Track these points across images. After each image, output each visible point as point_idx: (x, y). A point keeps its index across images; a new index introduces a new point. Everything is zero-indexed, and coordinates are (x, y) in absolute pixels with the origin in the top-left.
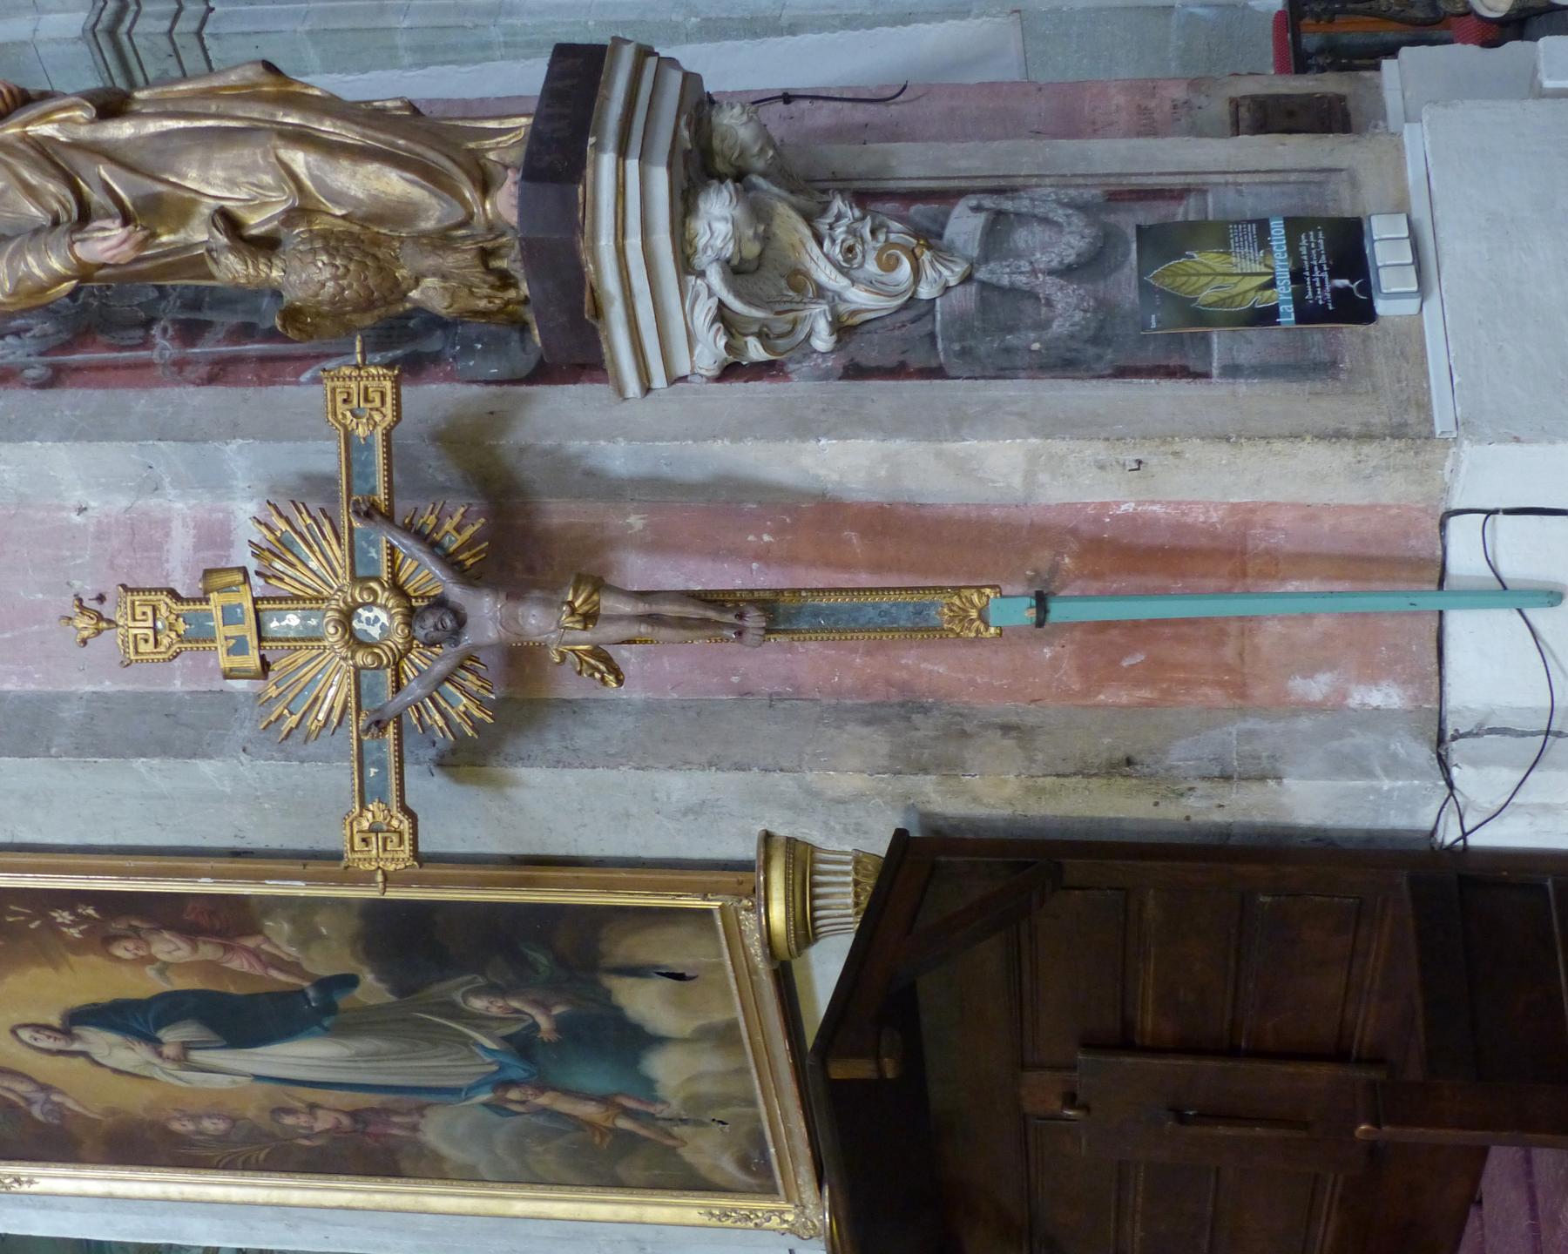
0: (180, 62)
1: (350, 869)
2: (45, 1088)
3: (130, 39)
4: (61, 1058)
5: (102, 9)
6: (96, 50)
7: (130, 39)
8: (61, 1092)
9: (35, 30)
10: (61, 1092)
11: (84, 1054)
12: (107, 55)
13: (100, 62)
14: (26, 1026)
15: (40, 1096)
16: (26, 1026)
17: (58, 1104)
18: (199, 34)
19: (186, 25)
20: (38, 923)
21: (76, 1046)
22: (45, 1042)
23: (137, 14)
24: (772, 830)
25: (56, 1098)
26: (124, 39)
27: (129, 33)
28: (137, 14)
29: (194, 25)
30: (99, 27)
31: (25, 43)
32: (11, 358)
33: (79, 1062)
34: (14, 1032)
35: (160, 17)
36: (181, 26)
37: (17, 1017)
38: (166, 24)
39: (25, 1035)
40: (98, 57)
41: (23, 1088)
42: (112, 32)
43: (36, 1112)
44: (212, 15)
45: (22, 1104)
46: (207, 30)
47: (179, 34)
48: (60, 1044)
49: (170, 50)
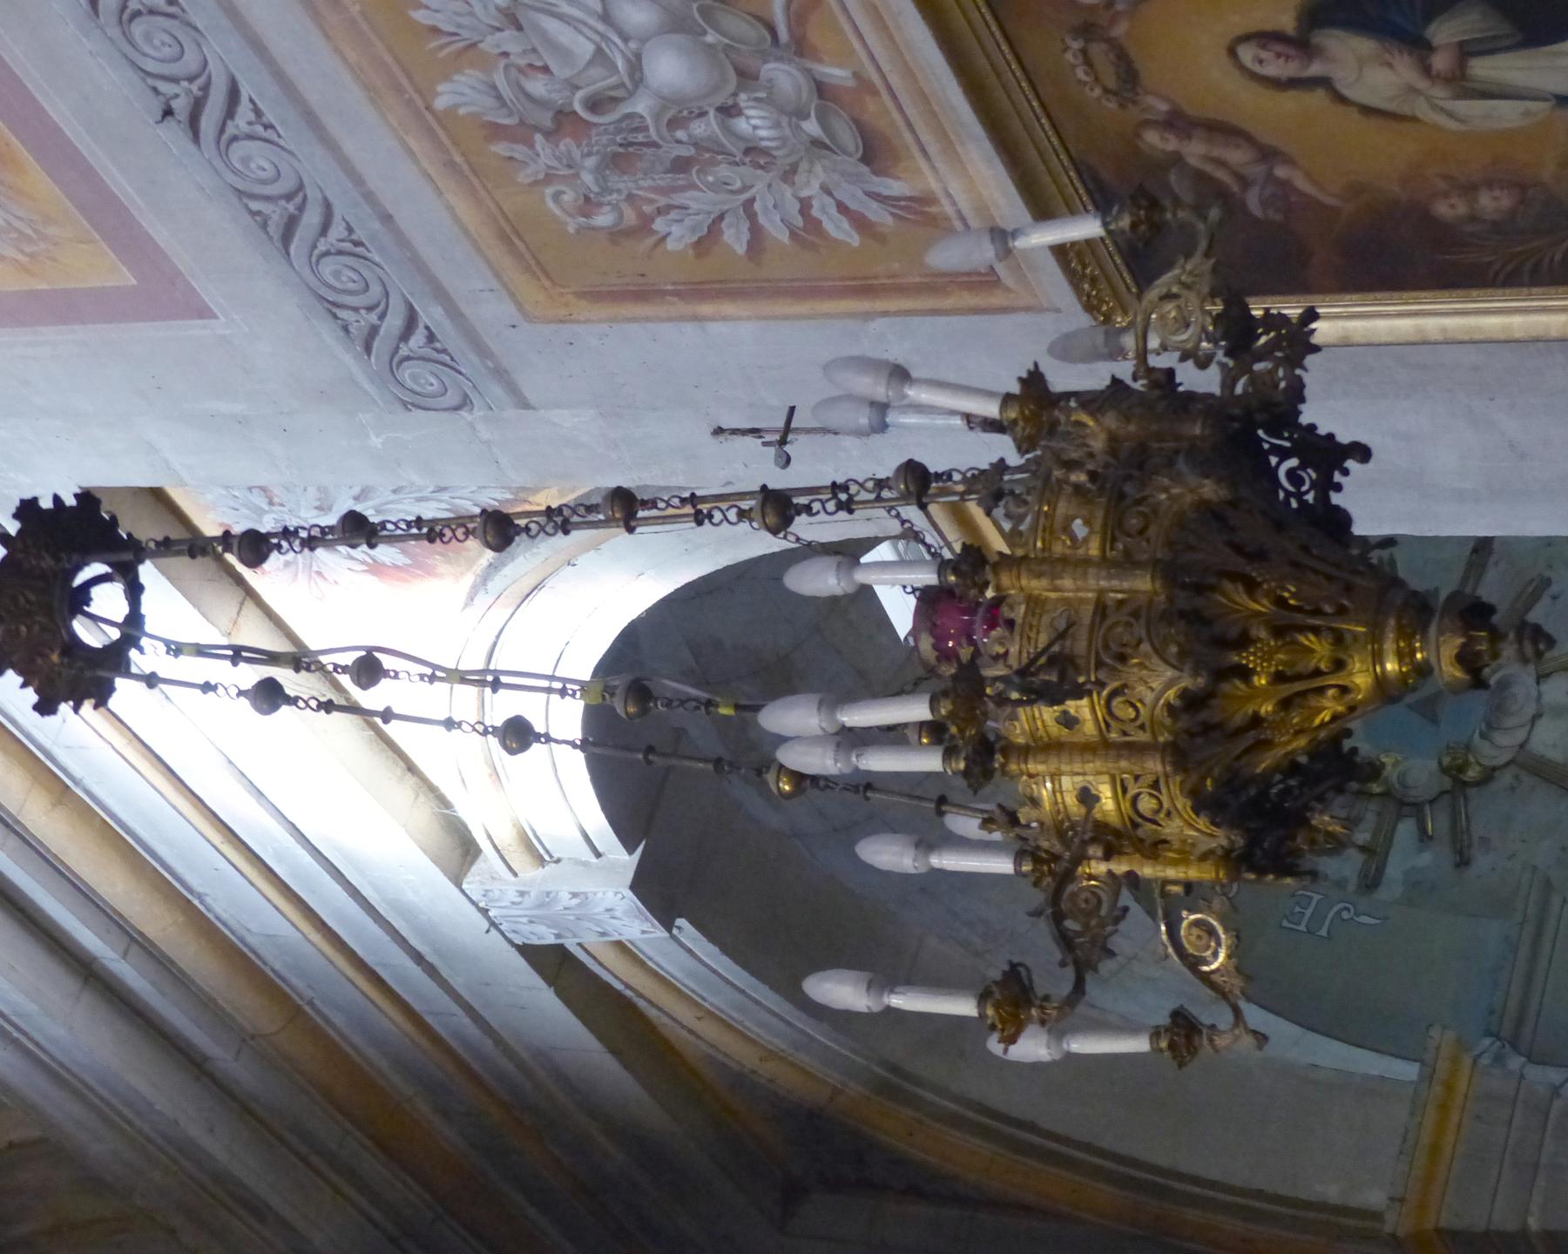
2: (1268, 154)
11: (1324, 82)
21: (1315, 69)
25: (1281, 172)
39: (1247, 54)
41: (1238, 156)
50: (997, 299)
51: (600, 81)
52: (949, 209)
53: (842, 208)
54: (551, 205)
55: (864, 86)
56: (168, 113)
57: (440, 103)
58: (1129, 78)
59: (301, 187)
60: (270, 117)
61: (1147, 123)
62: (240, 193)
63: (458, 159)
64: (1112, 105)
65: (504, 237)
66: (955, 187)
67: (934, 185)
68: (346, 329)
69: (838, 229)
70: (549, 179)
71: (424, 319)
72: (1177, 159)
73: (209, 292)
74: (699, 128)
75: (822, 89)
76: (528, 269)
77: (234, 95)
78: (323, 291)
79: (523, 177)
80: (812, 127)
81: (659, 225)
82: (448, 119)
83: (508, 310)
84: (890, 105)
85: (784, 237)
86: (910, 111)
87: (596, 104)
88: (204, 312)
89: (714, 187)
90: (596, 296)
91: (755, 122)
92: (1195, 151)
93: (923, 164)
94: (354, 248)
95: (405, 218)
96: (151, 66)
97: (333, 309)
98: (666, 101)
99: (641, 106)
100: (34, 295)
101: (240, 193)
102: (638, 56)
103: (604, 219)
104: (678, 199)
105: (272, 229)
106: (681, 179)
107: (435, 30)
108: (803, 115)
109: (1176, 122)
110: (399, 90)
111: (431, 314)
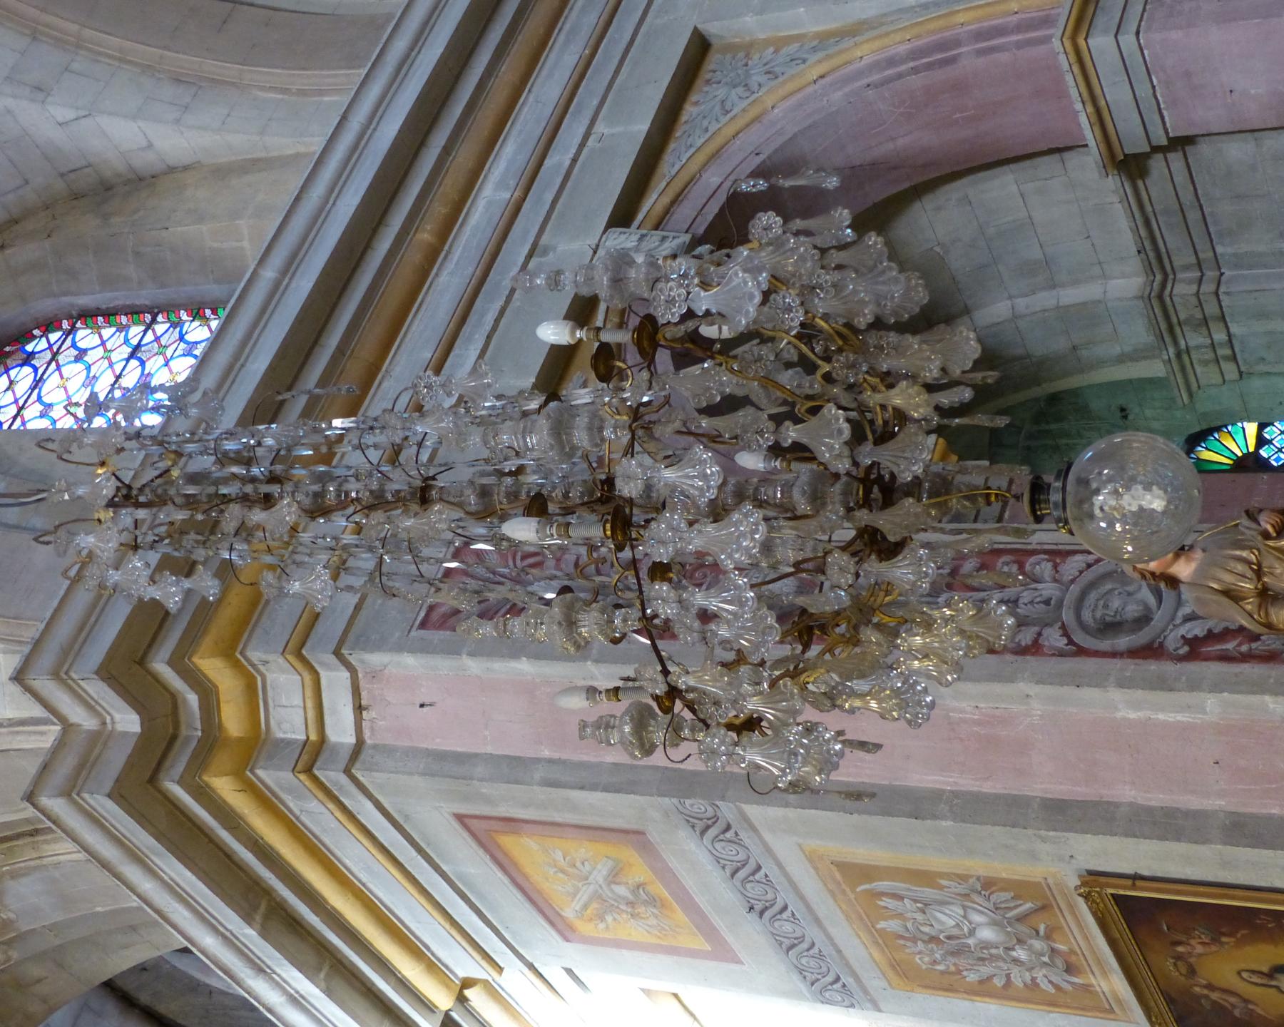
0: (1203, 310)
1: (46, 235)
2: (1246, 1001)
3: (1171, 299)
4: (1263, 988)
5: (1153, 281)
6: (1149, 308)
7: (1171, 299)
8: (1256, 1004)
9: (1105, 292)
10: (1256, 1004)
11: (1277, 988)
12: (1156, 311)
13: (1152, 315)
14: (1247, 971)
15: (1243, 1005)
16: (1247, 971)
17: (1252, 1010)
18: (1217, 294)
19: (1208, 287)
20: (1273, 925)
21: (1273, 983)
22: (1255, 979)
23: (1174, 280)
24: (712, 29)
25: (1251, 1007)
26: (1168, 300)
27: (1171, 296)
28: (1174, 280)
29: (1212, 287)
30: (1153, 294)
31: (1100, 301)
32: (1274, 646)
33: (1272, 991)
34: (1239, 973)
35: (1190, 282)
36: (1204, 288)
37: (1243, 966)
38: (1195, 287)
39: (1245, 975)
40: (1151, 312)
41: (1233, 1000)
42: (1160, 297)
43: (1237, 1013)
44: (1223, 278)
45: (1230, 1007)
46: (1222, 289)
47: (1204, 294)
48: (1264, 981)
49: (1197, 304)
50: (1112, 1016)
51: (955, 932)
52: (1098, 989)
53: (1050, 982)
54: (919, 961)
55: (1072, 952)
56: (751, 908)
57: (879, 926)
58: (1192, 972)
59: (804, 936)
60: (798, 916)
61: (1196, 985)
62: (773, 934)
63: (880, 941)
64: (1183, 978)
65: (893, 967)
66: (1103, 984)
67: (1094, 982)
68: (805, 978)
69: (1045, 985)
70: (920, 953)
71: (843, 980)
72: (1207, 997)
73: (742, 956)
74: (994, 951)
75: (1053, 950)
76: (899, 975)
77: (813, 945)
78: (715, 852)
79: (907, 951)
80: (1046, 959)
81: (965, 973)
82: (882, 932)
83: (884, 984)
84: (1082, 959)
85: (1021, 985)
86: (1091, 962)
87: (949, 938)
88: (739, 962)
89: (994, 967)
90: (926, 987)
91: (1020, 953)
92: (1215, 996)
93: (1091, 976)
94: (821, 955)
95: (848, 953)
96: (749, 895)
97: (801, 972)
98: (982, 942)
99: (971, 941)
100: (661, 946)
101: (773, 934)
102: (975, 928)
103: (941, 967)
104: (976, 968)
105: (783, 946)
106: (981, 963)
107: (886, 908)
108: (1043, 955)
109: (1210, 987)
110: (861, 919)
111: (768, 868)
